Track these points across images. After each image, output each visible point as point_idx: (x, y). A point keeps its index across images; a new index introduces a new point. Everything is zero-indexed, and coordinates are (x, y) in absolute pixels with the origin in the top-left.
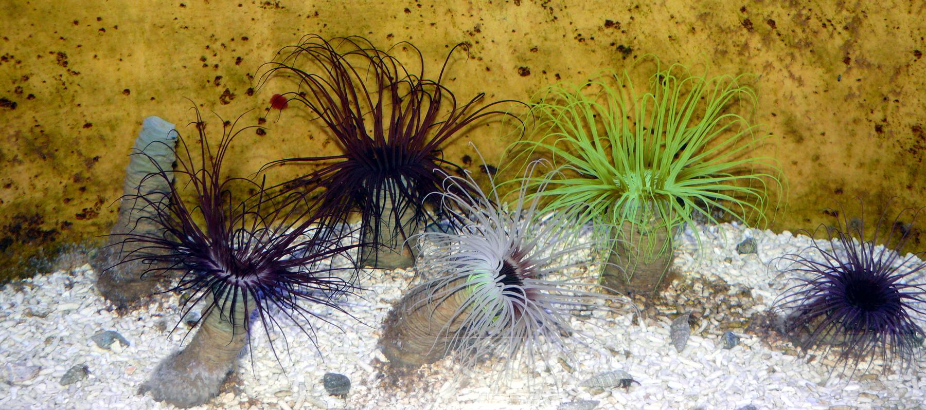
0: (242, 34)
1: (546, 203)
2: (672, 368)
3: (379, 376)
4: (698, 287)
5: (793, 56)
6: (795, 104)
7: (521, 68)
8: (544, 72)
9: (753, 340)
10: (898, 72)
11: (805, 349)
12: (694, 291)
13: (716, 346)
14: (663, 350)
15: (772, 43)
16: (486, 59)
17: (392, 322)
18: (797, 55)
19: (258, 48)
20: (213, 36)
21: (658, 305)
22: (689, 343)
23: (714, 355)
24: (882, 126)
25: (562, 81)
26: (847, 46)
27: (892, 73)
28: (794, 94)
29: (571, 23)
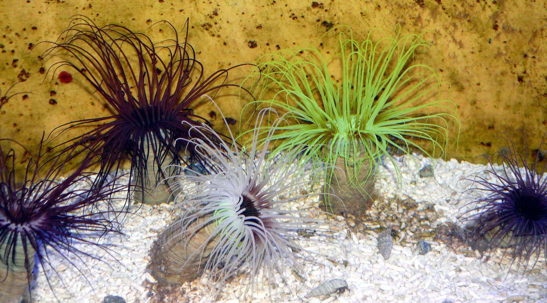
0: (31, 25)
1: (275, 144)
2: (381, 274)
3: (150, 295)
4: (394, 205)
5: (455, 25)
6: (457, 62)
7: (250, 42)
8: (268, 44)
9: (441, 247)
10: (535, 34)
11: (481, 252)
12: (391, 208)
13: (413, 252)
14: (373, 259)
15: (438, 16)
16: (223, 36)
17: (157, 251)
18: (458, 24)
19: (46, 35)
20: (8, 27)
21: (365, 221)
22: (393, 251)
23: (412, 260)
24: (523, 77)
25: (282, 50)
26: (496, 16)
27: (530, 36)
28: (457, 54)
29: (286, 5)
